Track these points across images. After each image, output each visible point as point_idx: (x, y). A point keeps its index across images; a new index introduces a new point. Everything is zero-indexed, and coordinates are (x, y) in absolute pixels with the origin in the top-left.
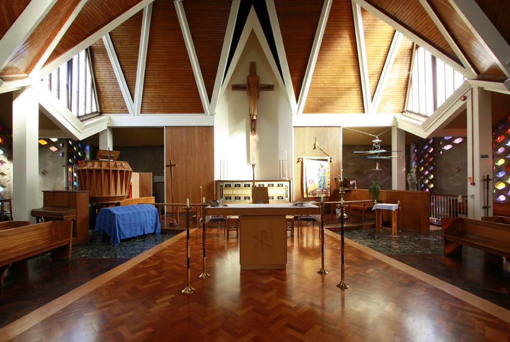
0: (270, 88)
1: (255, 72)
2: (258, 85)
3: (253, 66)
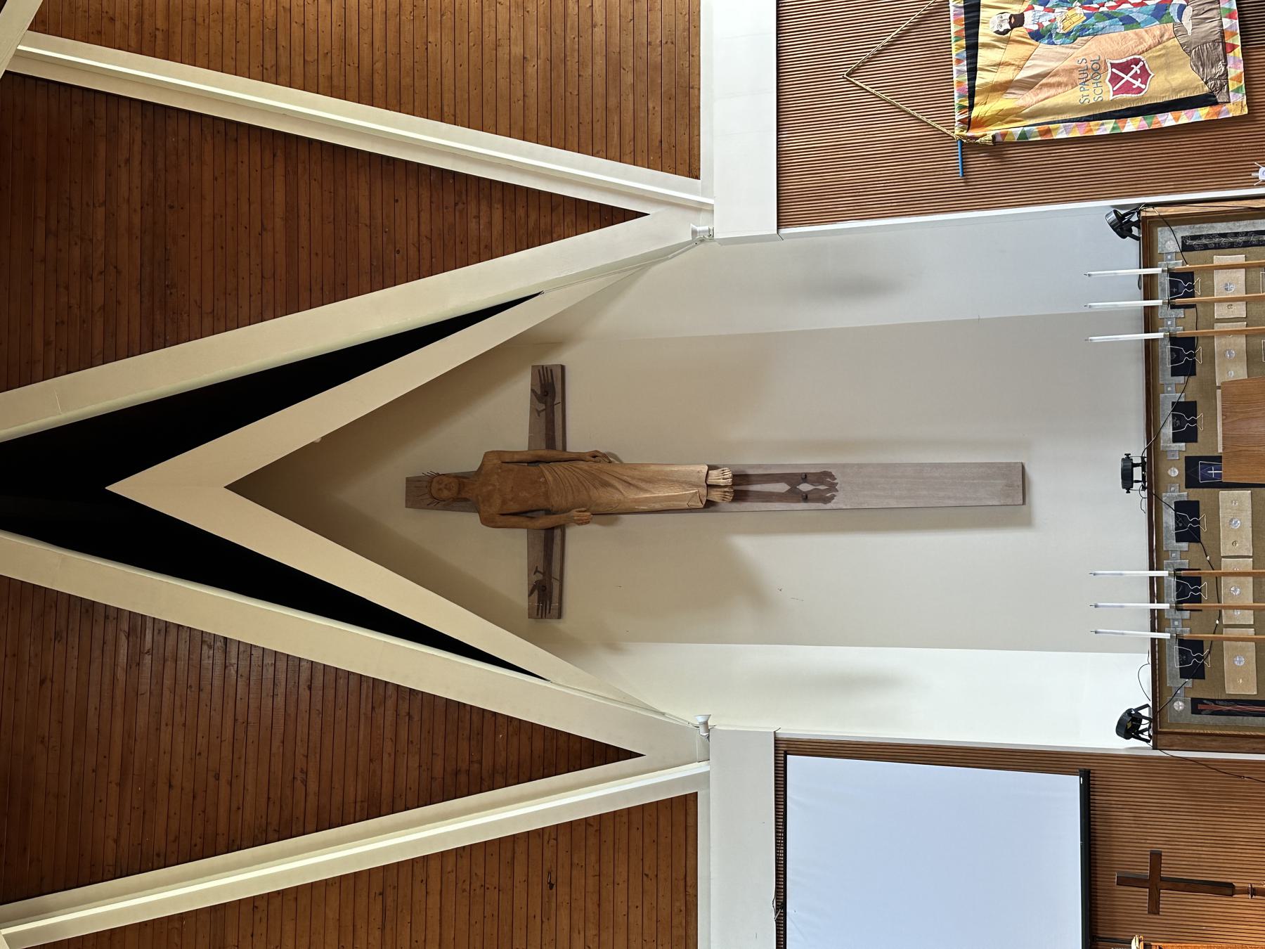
1: (461, 479)
2: (535, 462)
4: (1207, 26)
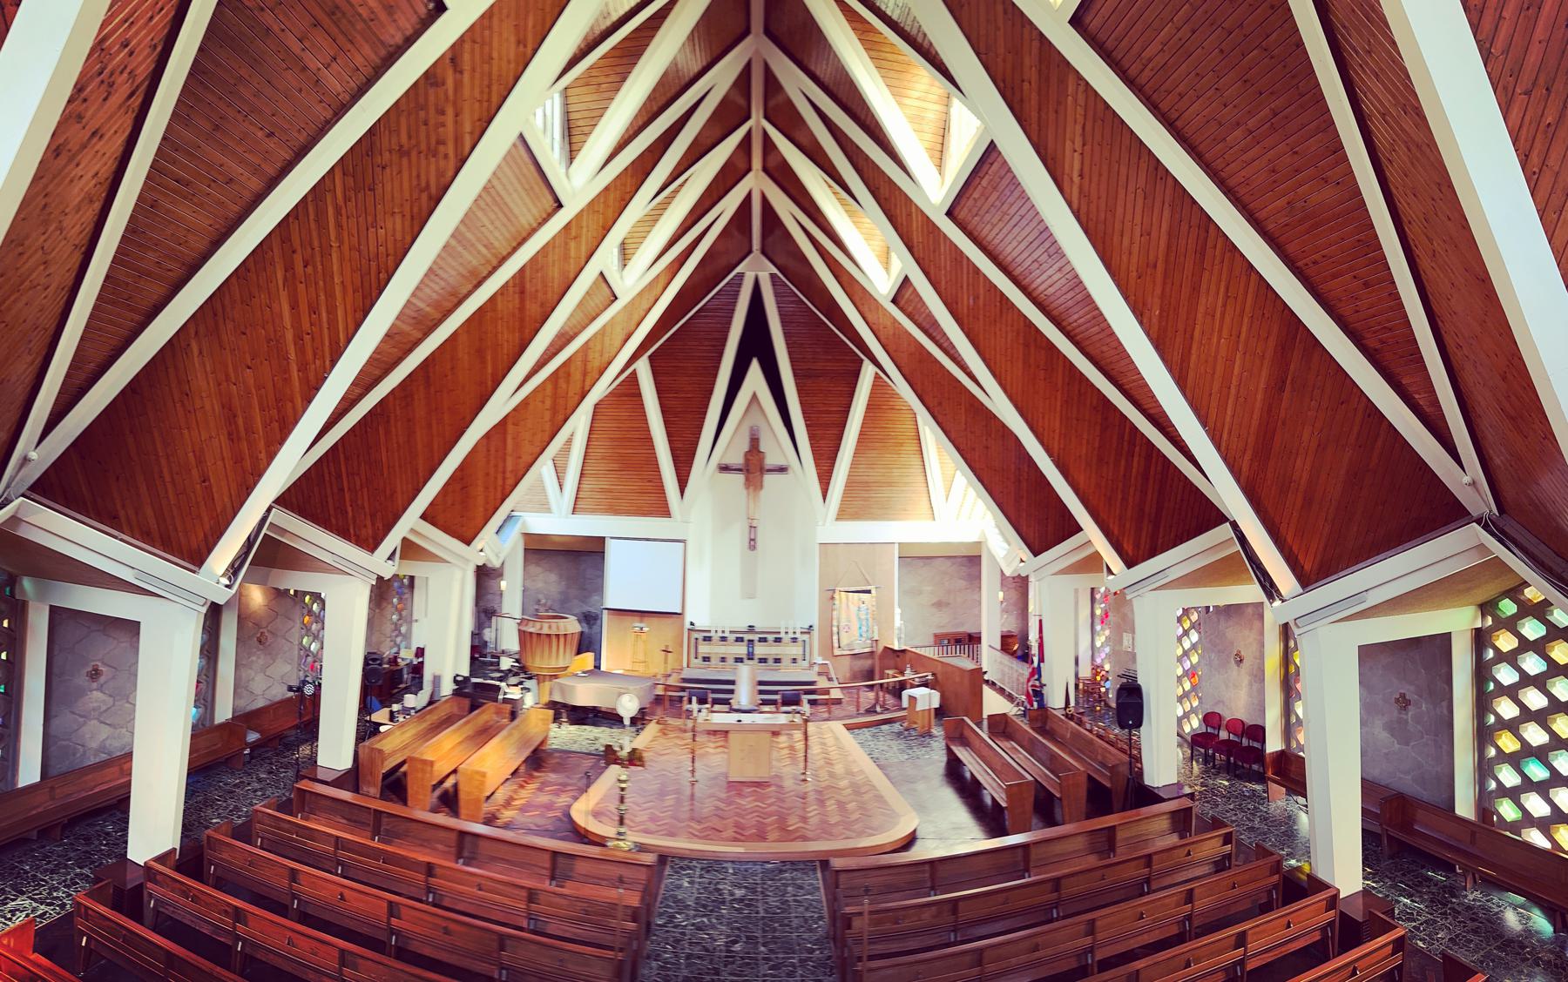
0: (782, 470)
3: (755, 442)
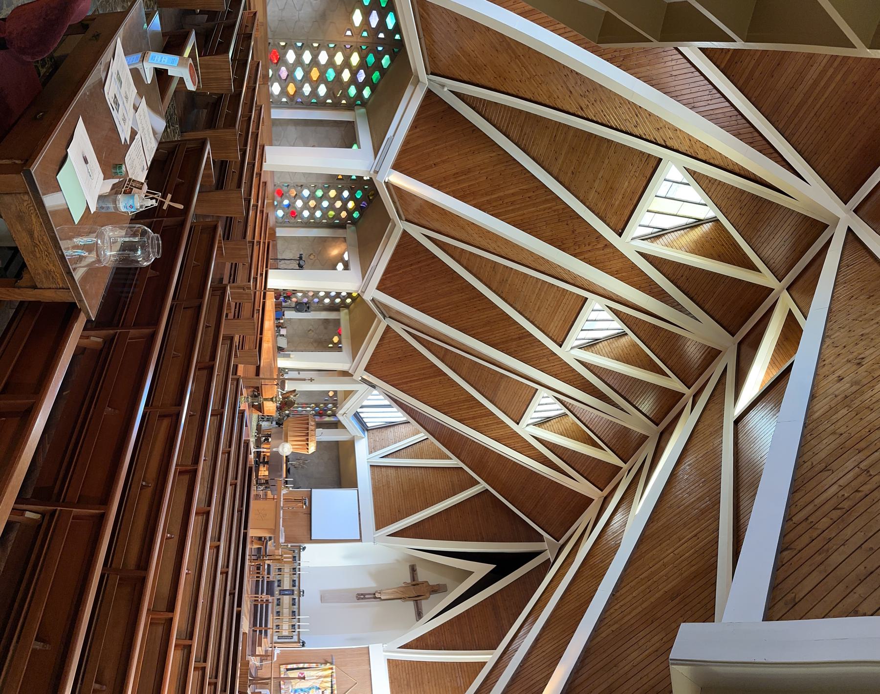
0: (419, 615)
4: (287, 687)
